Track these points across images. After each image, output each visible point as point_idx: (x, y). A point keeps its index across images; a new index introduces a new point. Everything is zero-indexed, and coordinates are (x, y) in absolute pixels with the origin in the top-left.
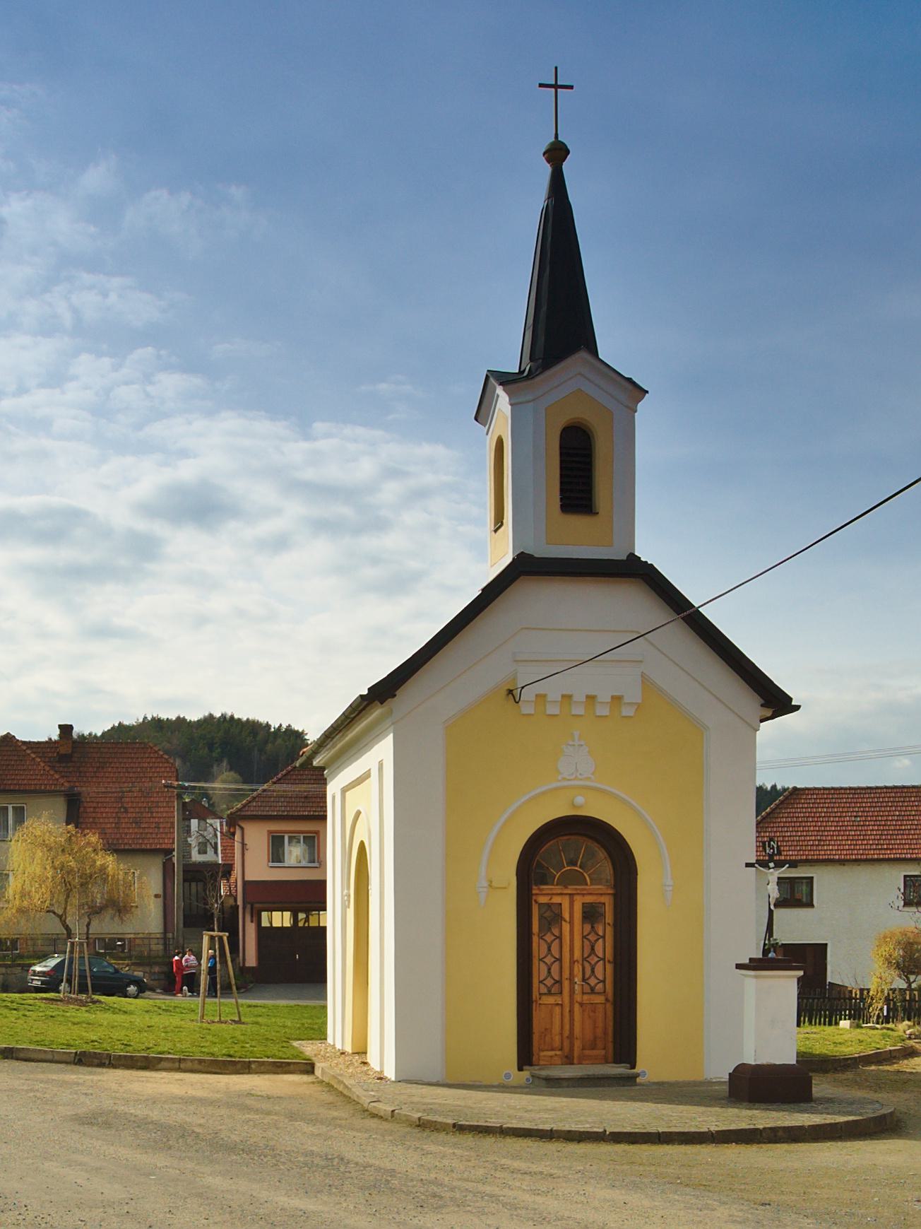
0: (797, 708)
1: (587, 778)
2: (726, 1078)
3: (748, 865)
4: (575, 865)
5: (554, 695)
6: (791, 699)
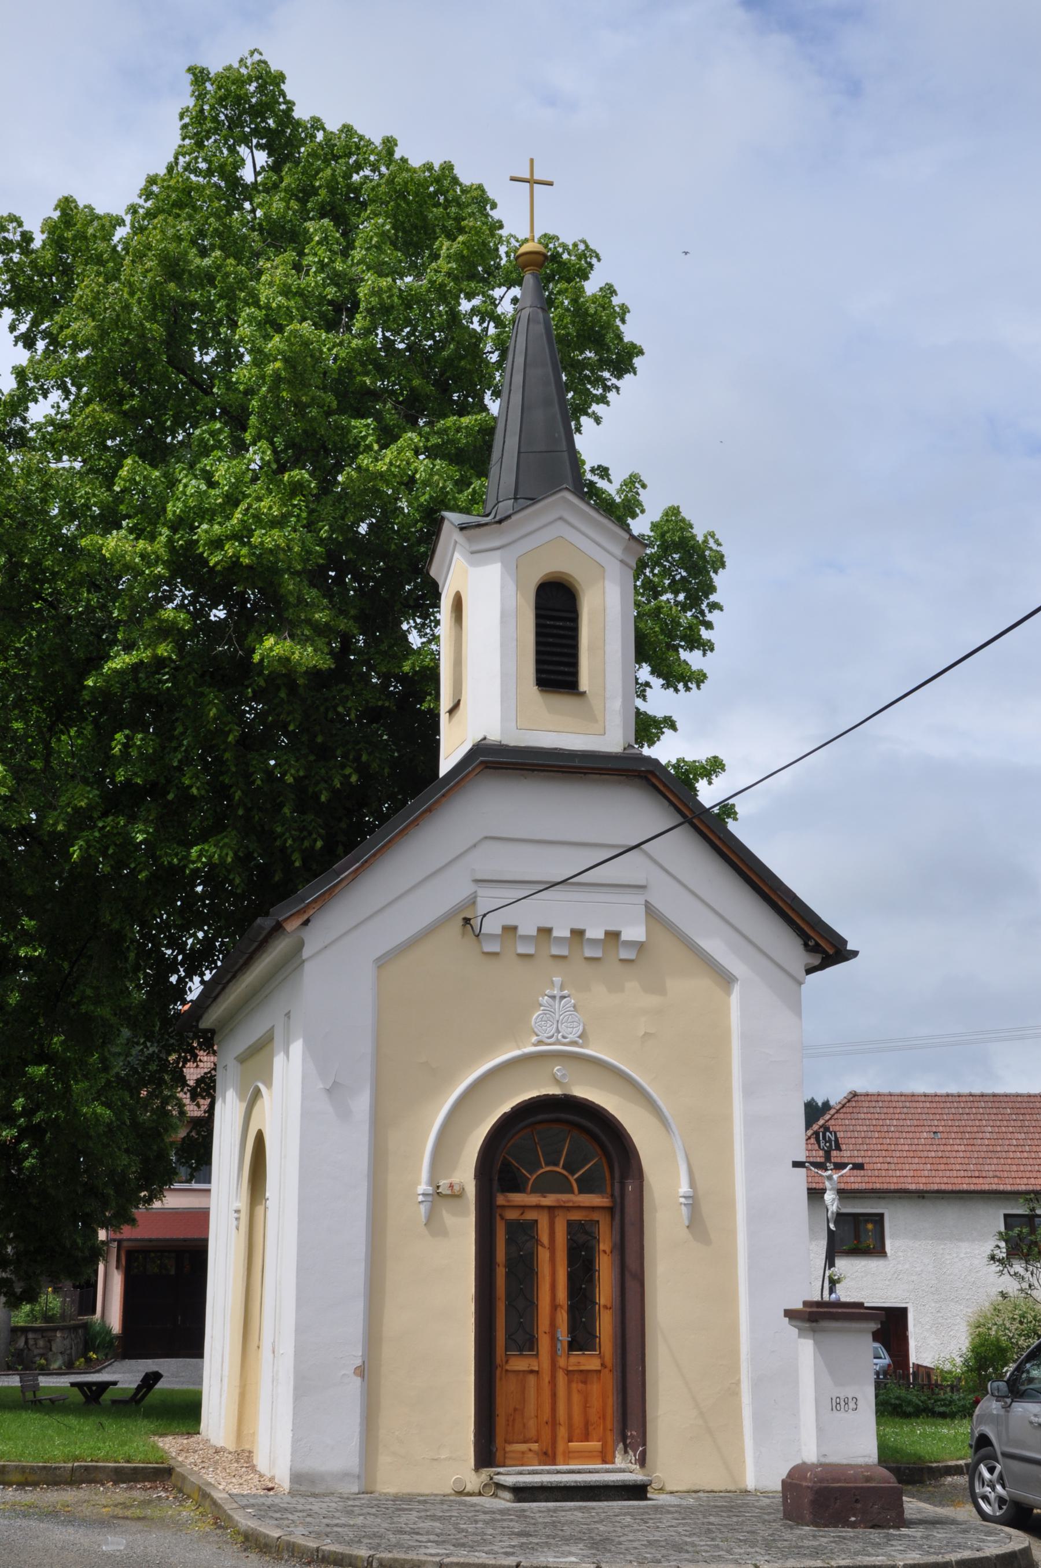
0: (855, 954)
1: (574, 1043)
2: (779, 1487)
3: (797, 1164)
4: (556, 1164)
5: (528, 928)
6: (845, 942)
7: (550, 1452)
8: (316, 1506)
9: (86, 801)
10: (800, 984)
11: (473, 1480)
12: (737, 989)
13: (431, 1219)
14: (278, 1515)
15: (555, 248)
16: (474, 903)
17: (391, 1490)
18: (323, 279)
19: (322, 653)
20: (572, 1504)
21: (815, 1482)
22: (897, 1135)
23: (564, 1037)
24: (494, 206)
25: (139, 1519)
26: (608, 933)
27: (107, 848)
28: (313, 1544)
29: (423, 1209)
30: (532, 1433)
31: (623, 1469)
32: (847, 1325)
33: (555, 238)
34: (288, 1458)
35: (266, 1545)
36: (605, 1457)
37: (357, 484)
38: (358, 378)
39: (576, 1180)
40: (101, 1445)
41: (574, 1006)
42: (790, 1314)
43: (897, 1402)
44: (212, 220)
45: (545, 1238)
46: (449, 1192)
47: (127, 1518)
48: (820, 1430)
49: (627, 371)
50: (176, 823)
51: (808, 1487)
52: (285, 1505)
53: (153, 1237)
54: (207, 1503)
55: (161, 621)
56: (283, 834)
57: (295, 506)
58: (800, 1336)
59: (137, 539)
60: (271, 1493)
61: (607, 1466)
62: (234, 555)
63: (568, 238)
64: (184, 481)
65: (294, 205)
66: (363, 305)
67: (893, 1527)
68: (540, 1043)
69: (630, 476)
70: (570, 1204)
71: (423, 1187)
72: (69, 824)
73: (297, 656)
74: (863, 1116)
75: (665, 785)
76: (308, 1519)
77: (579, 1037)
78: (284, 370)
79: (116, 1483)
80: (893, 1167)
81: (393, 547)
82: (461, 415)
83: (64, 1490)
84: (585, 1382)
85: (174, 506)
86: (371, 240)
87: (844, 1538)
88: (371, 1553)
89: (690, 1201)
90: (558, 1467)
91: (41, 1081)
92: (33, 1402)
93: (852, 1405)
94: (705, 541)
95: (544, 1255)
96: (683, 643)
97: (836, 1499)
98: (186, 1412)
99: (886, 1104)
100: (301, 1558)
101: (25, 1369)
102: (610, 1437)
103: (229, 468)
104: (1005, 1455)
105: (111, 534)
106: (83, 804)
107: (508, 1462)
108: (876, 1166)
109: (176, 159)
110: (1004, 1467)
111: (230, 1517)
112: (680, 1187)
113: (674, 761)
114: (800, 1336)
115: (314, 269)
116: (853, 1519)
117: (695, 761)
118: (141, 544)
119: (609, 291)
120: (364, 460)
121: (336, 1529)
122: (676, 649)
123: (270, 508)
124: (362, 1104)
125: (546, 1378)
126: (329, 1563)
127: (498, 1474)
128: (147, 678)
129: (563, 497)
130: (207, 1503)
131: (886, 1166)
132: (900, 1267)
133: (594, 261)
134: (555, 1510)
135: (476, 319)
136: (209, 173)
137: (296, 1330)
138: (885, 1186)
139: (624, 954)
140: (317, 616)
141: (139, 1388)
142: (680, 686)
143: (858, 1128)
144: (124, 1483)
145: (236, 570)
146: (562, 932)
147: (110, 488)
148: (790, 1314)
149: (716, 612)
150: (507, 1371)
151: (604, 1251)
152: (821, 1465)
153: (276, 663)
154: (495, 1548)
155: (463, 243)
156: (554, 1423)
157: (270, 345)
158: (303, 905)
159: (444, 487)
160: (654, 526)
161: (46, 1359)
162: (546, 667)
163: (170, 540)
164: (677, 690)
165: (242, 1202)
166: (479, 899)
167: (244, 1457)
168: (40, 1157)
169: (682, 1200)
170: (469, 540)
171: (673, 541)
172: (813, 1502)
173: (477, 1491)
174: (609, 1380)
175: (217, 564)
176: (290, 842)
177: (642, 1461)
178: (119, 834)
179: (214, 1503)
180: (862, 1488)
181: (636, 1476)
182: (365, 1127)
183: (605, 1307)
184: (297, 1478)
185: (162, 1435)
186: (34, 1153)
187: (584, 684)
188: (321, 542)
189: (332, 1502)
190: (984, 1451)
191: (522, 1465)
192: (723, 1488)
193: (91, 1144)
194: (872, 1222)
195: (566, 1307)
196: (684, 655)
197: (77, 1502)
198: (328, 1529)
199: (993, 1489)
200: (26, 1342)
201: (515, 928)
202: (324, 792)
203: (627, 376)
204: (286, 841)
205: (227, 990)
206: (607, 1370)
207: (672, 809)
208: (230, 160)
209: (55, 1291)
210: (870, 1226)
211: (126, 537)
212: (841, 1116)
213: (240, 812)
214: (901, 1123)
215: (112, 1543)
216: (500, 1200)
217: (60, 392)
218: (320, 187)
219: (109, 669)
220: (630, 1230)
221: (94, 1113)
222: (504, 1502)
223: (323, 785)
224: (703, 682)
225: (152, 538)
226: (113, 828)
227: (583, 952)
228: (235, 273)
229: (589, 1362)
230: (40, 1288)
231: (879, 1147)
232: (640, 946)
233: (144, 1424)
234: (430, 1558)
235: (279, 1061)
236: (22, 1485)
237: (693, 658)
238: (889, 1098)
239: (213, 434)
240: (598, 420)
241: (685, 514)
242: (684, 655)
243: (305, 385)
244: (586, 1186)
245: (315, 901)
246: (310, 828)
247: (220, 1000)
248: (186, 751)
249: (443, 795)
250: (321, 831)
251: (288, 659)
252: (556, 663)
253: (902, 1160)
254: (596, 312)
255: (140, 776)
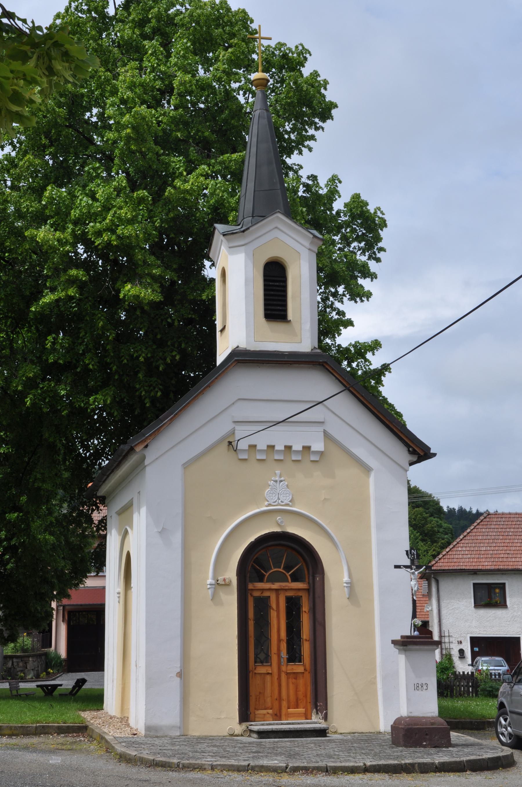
0: (434, 455)
1: (287, 505)
2: (389, 729)
4: (280, 567)
5: (262, 446)
6: (429, 449)
7: (278, 714)
8: (157, 742)
9: (33, 373)
10: (406, 471)
11: (238, 729)
12: (372, 474)
13: (214, 597)
14: (137, 746)
15: (285, 50)
16: (234, 433)
17: (197, 734)
18: (154, 76)
19: (157, 292)
20: (288, 739)
21: (405, 726)
22: (513, 537)
23: (282, 502)
24: (252, 21)
25: (69, 750)
26: (304, 447)
27: (45, 399)
28: (151, 758)
29: (210, 592)
30: (269, 705)
31: (316, 722)
32: (421, 647)
33: (285, 44)
34: (144, 719)
35: (130, 759)
36: (307, 716)
37: (175, 196)
38: (174, 133)
39: (290, 575)
40: (51, 715)
41: (287, 486)
42: (394, 642)
43: (490, 689)
44: (91, 41)
45: (274, 606)
46: (223, 583)
47: (63, 749)
48: (408, 700)
49: (328, 118)
50: (82, 384)
51: (402, 728)
52: (141, 742)
53: (83, 603)
54: (103, 742)
55: (70, 276)
56: (140, 389)
57: (140, 210)
58: (399, 654)
59: (56, 230)
60: (136, 736)
61: (308, 721)
62: (108, 240)
63: (291, 44)
64: (80, 198)
65: (137, 32)
66: (176, 91)
67: (445, 747)
68: (269, 505)
69: (332, 176)
70: (287, 588)
71: (210, 581)
72: (25, 386)
73: (142, 295)
74: (493, 527)
75: (333, 369)
76: (152, 747)
77: (290, 501)
78: (132, 133)
79: (58, 734)
80: (510, 556)
81: (195, 230)
82: (232, 153)
83: (32, 738)
84: (296, 678)
85: (75, 212)
86: (180, 52)
87: (416, 752)
88: (179, 761)
89: (349, 585)
90: (282, 722)
91: (15, 521)
92: (16, 695)
93: (425, 687)
94: (375, 212)
95: (273, 614)
96: (360, 275)
97: (416, 734)
98: (97, 699)
99: (507, 519)
100: (146, 764)
101: (12, 679)
102: (309, 707)
103: (104, 191)
104: (511, 712)
105: (41, 228)
106: (31, 375)
107: (257, 719)
108: (500, 556)
109: (70, 4)
110: (511, 718)
111: (113, 747)
112: (344, 578)
113: (353, 343)
114: (399, 654)
115: (149, 70)
116: (425, 743)
117: (365, 343)
118: (58, 234)
119: (315, 74)
120: (178, 183)
121: (164, 751)
122: (356, 278)
123: (126, 213)
124: (177, 538)
125: (276, 677)
126: (159, 766)
127: (251, 725)
128: (64, 305)
129: (278, 217)
130: (103, 742)
131: (506, 556)
132: (515, 614)
133: (308, 56)
134: (277, 742)
135: (241, 92)
136: (89, 11)
137: (146, 654)
138: (506, 567)
139: (313, 458)
140: (154, 271)
141: (74, 687)
142: (358, 299)
143: (490, 534)
144: (62, 734)
145: (109, 247)
146: (280, 447)
147: (40, 202)
148: (394, 642)
149: (382, 253)
150: (255, 673)
151: (305, 612)
152: (409, 717)
153: (132, 298)
154: (240, 758)
155: (232, 53)
156: (280, 699)
157: (124, 120)
158: (144, 438)
159: (222, 196)
160: (346, 205)
161: (24, 673)
162: (270, 307)
163: (73, 231)
164: (356, 302)
165: (121, 589)
166: (236, 431)
167: (124, 720)
168: (16, 562)
169: (345, 585)
170: (228, 241)
171: (357, 214)
172: (405, 735)
173: (240, 734)
174: (308, 677)
175: (99, 245)
176: (143, 393)
177: (326, 718)
178: (52, 391)
179: (107, 741)
180: (429, 728)
181: (322, 725)
182: (179, 551)
183: (306, 640)
184: (148, 728)
185: (84, 710)
186: (12, 561)
187: (290, 316)
188: (156, 229)
189: (166, 740)
190: (502, 710)
191: (264, 721)
192: (368, 731)
193: (43, 556)
194: (498, 588)
195: (285, 641)
196: (360, 281)
197: (38, 743)
198: (160, 751)
199: (507, 729)
200: (13, 664)
201: (255, 446)
202: (161, 365)
203: (329, 121)
204: (141, 392)
205: (110, 477)
206: (307, 672)
207: (337, 381)
208: (101, 4)
209: (27, 636)
210: (497, 591)
211: (49, 230)
212: (481, 527)
213: (116, 377)
214: (516, 530)
215: (54, 759)
216: (250, 586)
217: (10, 147)
218: (152, 18)
219: (43, 302)
220: (318, 601)
221: (44, 538)
222: (254, 738)
223: (161, 361)
224: (370, 297)
225: (63, 229)
226: (48, 388)
227: (291, 458)
228: (105, 76)
229: (298, 668)
230: (18, 634)
231: (503, 544)
232: (321, 453)
233: (75, 705)
234: (207, 763)
235: (135, 516)
236: (10, 736)
237: (365, 283)
238: (509, 516)
239: (95, 169)
240: (310, 149)
241: (363, 197)
242: (360, 281)
243: (144, 141)
244: (295, 578)
245: (150, 435)
246: (154, 385)
247: (107, 482)
248: (86, 345)
249: (216, 378)
250: (161, 387)
251: (138, 296)
252: (275, 306)
253: (516, 552)
254: (307, 89)
255: (62, 359)
